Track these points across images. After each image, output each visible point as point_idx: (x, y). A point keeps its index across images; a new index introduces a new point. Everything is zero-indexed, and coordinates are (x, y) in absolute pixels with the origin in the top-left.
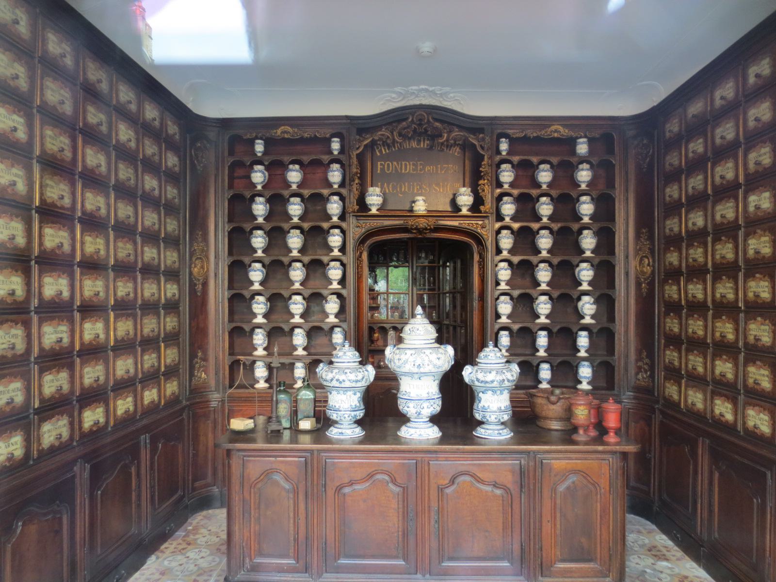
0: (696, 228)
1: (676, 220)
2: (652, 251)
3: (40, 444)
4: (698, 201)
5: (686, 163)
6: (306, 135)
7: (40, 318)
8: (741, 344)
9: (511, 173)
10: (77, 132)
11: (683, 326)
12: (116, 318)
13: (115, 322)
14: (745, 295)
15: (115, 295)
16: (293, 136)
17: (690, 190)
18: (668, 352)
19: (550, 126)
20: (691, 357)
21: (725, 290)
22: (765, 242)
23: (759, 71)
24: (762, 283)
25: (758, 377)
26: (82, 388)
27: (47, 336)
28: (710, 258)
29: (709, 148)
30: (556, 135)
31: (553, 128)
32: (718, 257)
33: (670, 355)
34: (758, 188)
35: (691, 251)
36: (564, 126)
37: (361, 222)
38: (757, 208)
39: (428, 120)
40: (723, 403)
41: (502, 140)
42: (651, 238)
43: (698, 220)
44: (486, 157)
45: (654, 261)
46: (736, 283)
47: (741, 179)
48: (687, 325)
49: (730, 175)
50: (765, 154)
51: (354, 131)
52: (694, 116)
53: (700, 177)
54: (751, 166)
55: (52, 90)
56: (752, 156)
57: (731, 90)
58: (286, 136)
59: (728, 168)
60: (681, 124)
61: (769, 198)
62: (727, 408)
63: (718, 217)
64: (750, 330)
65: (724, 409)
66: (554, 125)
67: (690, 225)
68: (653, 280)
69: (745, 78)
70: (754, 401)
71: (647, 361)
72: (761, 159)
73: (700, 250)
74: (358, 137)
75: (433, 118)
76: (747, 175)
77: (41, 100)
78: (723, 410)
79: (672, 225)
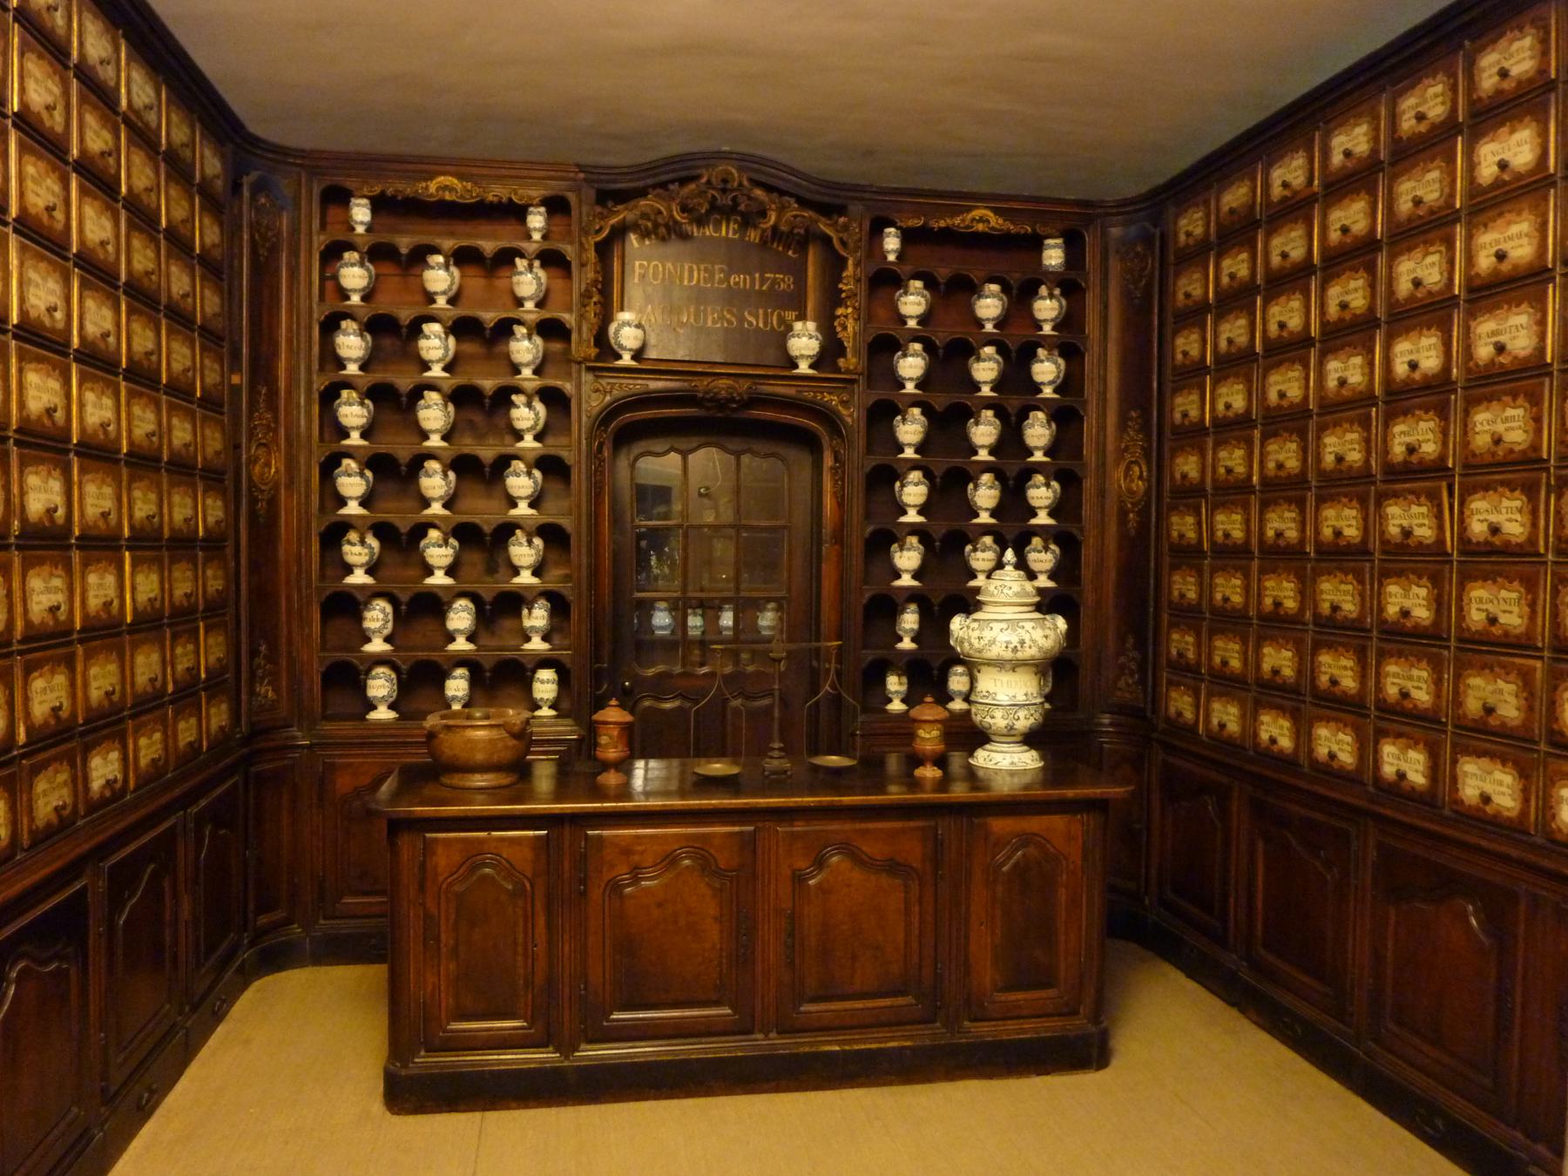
0: (1230, 414)
1: (1195, 397)
2: (1147, 453)
3: (32, 819)
4: (1235, 363)
5: (1216, 293)
6: (490, 198)
7: (24, 559)
8: (1308, 615)
9: (919, 299)
10: (69, 168)
11: (1206, 589)
12: (134, 565)
13: (133, 574)
14: (1317, 532)
15: (131, 517)
16: (462, 197)
17: (1223, 345)
18: (1175, 636)
19: (969, 209)
20: (1219, 643)
21: (1282, 523)
22: (1352, 442)
23: (1349, 146)
24: (1347, 512)
25: (1336, 672)
26: (88, 709)
27: (35, 598)
28: (1256, 467)
29: (1260, 269)
30: (980, 227)
31: (976, 213)
32: (1271, 465)
33: (1179, 642)
34: (1342, 348)
35: (1223, 454)
36: (996, 211)
37: (604, 382)
38: (1342, 382)
39: (741, 185)
40: (1275, 721)
41: (888, 230)
42: (1145, 428)
43: (1233, 397)
44: (850, 262)
45: (1150, 471)
46: (1302, 512)
47: (1314, 331)
48: (1212, 588)
49: (1295, 323)
50: (1356, 290)
51: (590, 193)
52: (1232, 211)
53: (1242, 322)
54: (1333, 310)
55: (37, 81)
56: (1335, 293)
57: (1300, 172)
58: (448, 197)
59: (1292, 310)
60: (1208, 224)
61: (1362, 367)
62: (1282, 728)
63: (1273, 396)
64: (1322, 592)
65: (1276, 730)
66: (977, 208)
67: (1221, 407)
68: (1148, 506)
69: (1326, 153)
70: (1328, 712)
71: (1135, 654)
72: (1348, 298)
73: (1239, 453)
74: (599, 209)
75: (751, 180)
76: (1324, 324)
77: (22, 102)
78: (1275, 732)
79: (1186, 405)
